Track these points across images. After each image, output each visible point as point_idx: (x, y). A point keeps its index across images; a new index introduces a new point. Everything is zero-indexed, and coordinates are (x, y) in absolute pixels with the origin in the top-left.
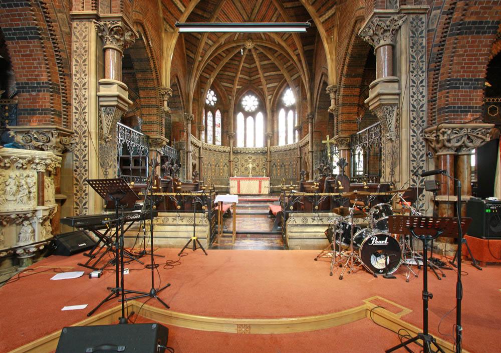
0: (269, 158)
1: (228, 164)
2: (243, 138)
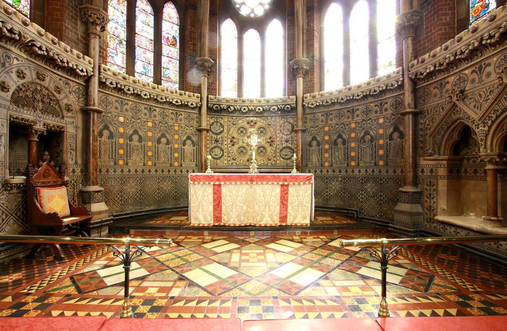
0: (300, 123)
1: (195, 139)
2: (300, 273)
